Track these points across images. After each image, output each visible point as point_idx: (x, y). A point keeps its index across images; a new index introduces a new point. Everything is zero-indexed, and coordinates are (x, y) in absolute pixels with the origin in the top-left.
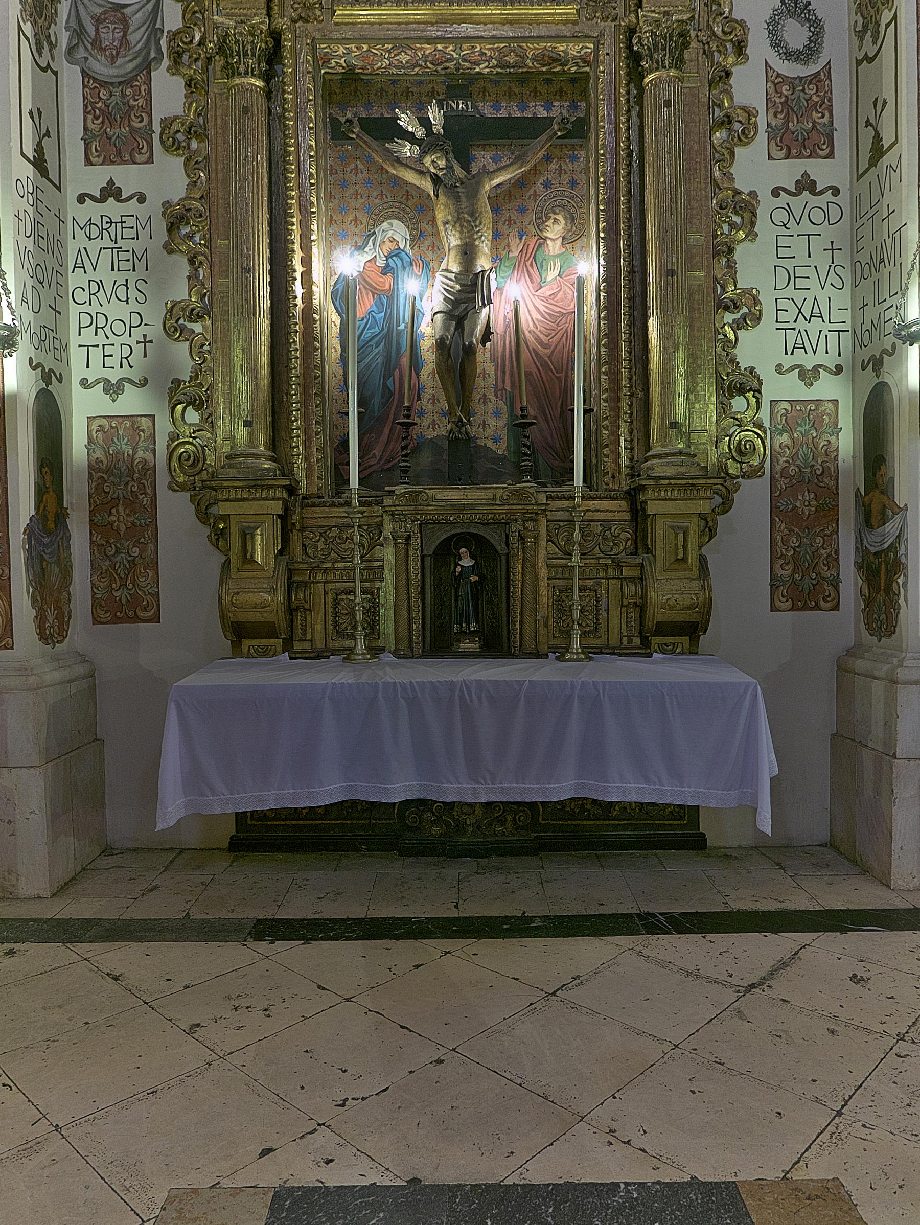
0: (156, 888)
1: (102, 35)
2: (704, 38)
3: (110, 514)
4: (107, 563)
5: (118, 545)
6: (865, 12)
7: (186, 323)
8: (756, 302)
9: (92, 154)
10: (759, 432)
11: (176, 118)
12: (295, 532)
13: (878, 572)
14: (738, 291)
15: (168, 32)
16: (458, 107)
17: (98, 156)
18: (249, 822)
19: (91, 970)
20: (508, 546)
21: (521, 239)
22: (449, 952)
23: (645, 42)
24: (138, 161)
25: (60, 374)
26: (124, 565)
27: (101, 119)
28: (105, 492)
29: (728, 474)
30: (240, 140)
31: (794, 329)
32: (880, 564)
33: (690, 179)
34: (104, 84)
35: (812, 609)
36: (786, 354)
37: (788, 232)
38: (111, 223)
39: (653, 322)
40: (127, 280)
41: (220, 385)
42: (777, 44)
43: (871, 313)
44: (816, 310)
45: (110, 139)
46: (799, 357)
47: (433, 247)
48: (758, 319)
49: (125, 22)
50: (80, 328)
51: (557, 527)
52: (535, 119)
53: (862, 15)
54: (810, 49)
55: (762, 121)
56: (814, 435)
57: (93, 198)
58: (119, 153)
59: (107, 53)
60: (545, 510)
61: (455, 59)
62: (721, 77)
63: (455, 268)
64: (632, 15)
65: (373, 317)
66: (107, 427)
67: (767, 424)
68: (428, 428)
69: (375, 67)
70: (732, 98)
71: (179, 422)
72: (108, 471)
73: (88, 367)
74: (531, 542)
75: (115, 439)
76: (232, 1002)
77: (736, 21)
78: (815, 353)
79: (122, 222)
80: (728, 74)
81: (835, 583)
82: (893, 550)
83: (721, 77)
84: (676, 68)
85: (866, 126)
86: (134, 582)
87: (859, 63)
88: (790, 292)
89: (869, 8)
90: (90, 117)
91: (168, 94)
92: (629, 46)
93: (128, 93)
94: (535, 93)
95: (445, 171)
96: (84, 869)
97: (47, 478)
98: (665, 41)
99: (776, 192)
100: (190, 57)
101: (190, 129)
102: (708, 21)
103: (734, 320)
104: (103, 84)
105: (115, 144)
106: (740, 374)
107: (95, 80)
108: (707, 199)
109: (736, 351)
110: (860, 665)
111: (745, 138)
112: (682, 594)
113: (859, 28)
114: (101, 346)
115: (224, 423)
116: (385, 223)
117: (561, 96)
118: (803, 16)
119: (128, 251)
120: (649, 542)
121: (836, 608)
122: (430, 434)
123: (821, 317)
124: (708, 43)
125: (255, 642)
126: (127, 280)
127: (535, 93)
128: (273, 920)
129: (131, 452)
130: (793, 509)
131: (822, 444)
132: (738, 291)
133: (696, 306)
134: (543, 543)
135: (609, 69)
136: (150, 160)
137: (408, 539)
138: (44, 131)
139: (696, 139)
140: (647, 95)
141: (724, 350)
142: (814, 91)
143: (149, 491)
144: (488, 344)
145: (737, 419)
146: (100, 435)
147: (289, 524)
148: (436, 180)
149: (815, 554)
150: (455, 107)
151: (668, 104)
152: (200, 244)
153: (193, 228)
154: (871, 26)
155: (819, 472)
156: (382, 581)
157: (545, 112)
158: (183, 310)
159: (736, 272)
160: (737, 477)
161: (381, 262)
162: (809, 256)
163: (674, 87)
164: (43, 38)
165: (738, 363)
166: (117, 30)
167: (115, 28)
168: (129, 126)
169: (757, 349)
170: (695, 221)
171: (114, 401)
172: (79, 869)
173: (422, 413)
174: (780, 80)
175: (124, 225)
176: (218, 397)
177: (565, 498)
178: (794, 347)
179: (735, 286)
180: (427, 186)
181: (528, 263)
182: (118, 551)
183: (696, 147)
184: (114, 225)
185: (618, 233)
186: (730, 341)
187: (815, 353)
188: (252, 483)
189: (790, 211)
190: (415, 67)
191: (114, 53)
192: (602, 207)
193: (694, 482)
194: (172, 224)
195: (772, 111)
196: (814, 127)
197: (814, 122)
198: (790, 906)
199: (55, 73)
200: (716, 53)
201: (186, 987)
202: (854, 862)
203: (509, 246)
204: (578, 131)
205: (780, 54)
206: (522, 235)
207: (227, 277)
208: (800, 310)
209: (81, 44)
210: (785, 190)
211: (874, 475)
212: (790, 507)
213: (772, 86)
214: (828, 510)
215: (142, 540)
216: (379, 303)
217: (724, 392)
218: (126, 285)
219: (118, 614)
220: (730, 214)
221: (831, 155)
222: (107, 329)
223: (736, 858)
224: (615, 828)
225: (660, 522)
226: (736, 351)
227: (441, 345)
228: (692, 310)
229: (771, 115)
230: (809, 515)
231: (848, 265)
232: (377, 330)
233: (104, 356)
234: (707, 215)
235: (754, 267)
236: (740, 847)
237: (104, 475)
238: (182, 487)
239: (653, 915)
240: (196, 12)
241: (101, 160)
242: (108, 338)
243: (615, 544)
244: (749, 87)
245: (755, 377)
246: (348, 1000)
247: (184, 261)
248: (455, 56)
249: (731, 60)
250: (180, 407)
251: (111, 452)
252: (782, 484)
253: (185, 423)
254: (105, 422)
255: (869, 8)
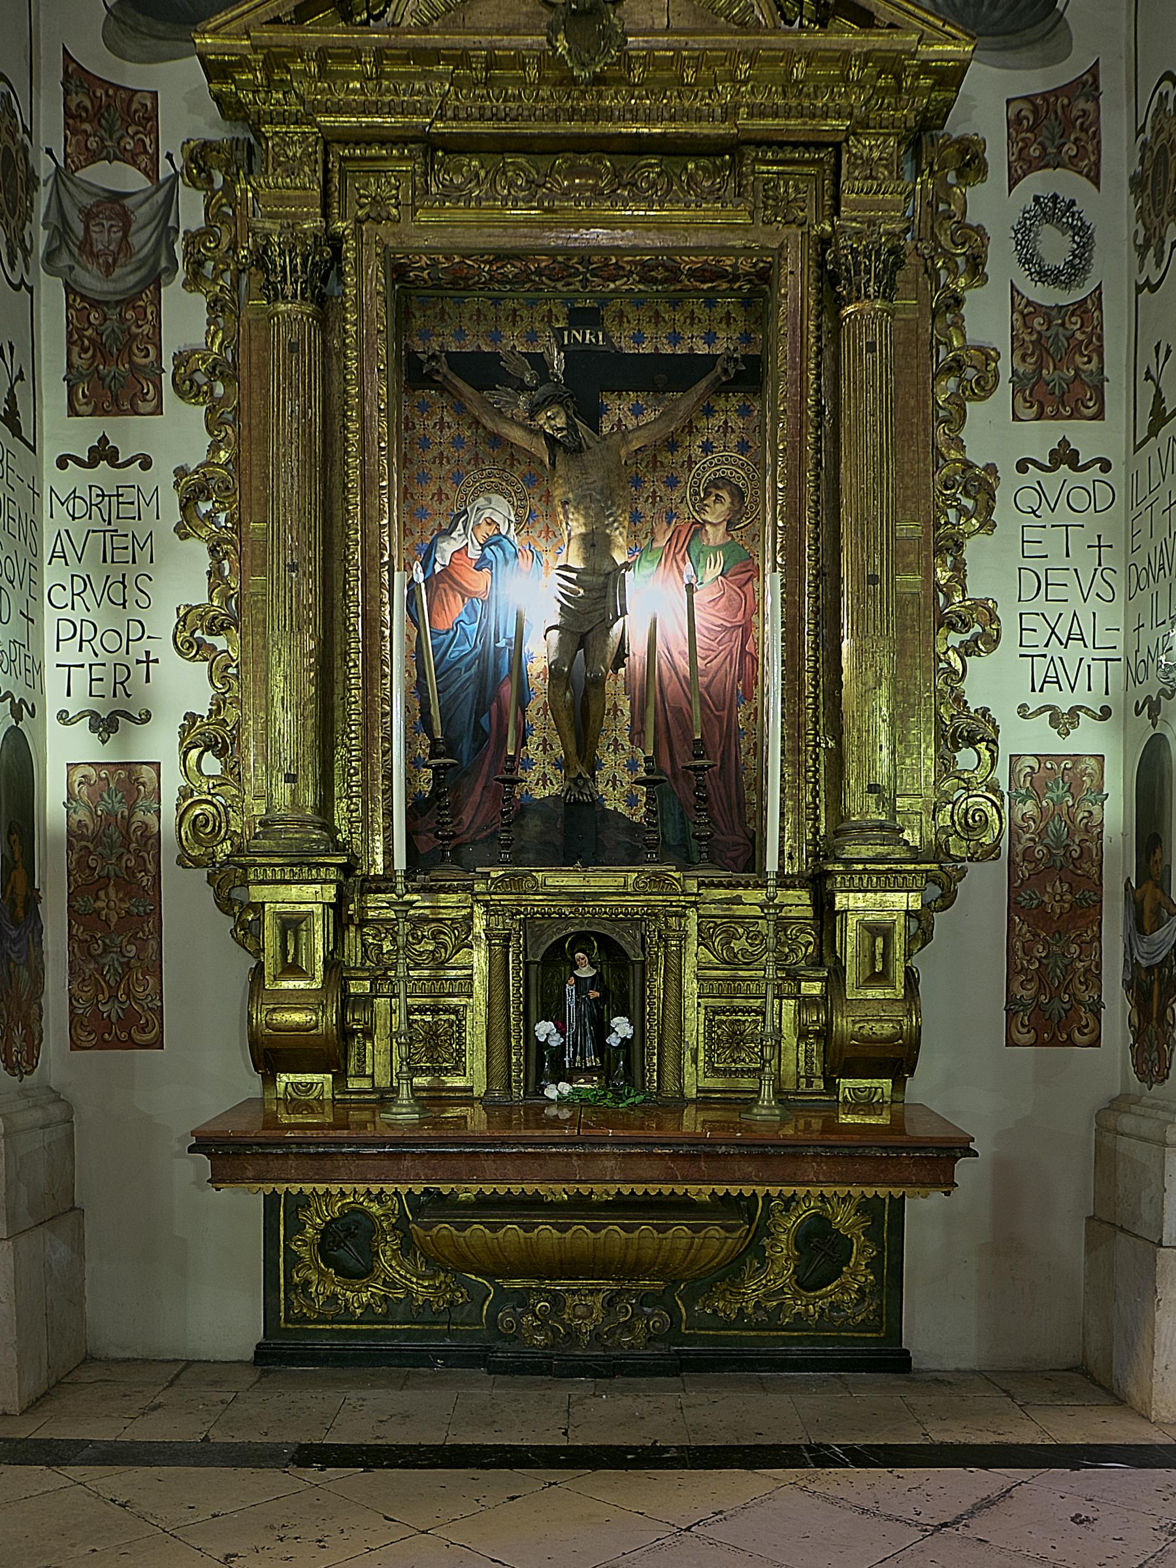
0: (160, 1406)
1: (94, 236)
2: (926, 251)
3: (97, 898)
4: (92, 966)
5: (107, 941)
6: (1148, 222)
7: (205, 637)
8: (993, 618)
9: (78, 400)
10: (994, 798)
11: (194, 352)
12: (352, 928)
13: (1150, 993)
14: (968, 603)
15: (185, 233)
16: (584, 339)
17: (86, 404)
18: (283, 1325)
19: (89, 1495)
20: (643, 949)
21: (669, 523)
22: (555, 1484)
23: (843, 260)
24: (142, 411)
25: (33, 706)
26: (116, 970)
27: (90, 352)
28: (89, 867)
29: (950, 856)
30: (284, 389)
31: (1044, 656)
32: (1152, 983)
33: (903, 447)
34: (95, 304)
35: (1063, 1044)
36: (1033, 690)
37: (1038, 522)
38: (103, 496)
39: (846, 645)
40: (124, 576)
41: (251, 722)
42: (1028, 259)
43: (1149, 637)
44: (1075, 630)
45: (103, 380)
46: (1051, 695)
47: (547, 533)
48: (994, 642)
49: (125, 218)
50: (58, 640)
51: (712, 925)
52: (692, 356)
53: (1144, 224)
54: (1073, 267)
55: (1005, 367)
56: (1070, 803)
57: (78, 461)
58: (115, 400)
59: (101, 261)
60: (694, 903)
61: (582, 273)
62: (948, 307)
63: (577, 563)
64: (827, 222)
65: (462, 628)
66: (94, 778)
67: (1004, 788)
68: (537, 784)
69: (470, 282)
70: (964, 336)
71: (193, 774)
72: (96, 839)
73: (69, 694)
74: (675, 946)
75: (105, 795)
76: (276, 1533)
77: (970, 227)
78: (1072, 689)
79: (118, 495)
80: (959, 302)
81: (1096, 1009)
82: (1168, 964)
83: (948, 307)
84: (884, 297)
85: (1146, 379)
86: (128, 994)
87: (1139, 289)
88: (1039, 605)
89: (1153, 216)
90: (76, 349)
91: (184, 320)
92: (821, 264)
93: (128, 317)
94: (693, 319)
95: (565, 433)
96: (59, 1382)
97: (16, 848)
98: (870, 260)
99: (1022, 466)
100: (214, 268)
101: (214, 368)
102: (932, 227)
103: (962, 642)
104: (95, 304)
105: (110, 388)
106: (968, 717)
107: (84, 298)
108: (927, 476)
109: (963, 686)
110: (1127, 1122)
111: (984, 387)
112: (880, 1020)
113: (1140, 241)
114: (87, 667)
115: (256, 776)
116: (481, 499)
117: (728, 324)
118: (1064, 220)
119: (126, 536)
120: (838, 950)
121: (1096, 1043)
122: (540, 793)
123: (1083, 639)
124: (932, 258)
125: (292, 1078)
126: (124, 576)
127: (693, 319)
128: (322, 1445)
129: (126, 813)
130: (1038, 906)
131: (1081, 816)
132: (968, 603)
133: (909, 623)
134: (692, 945)
135: (795, 287)
136: (158, 410)
137: (507, 939)
138: (16, 372)
139: (913, 391)
140: (844, 333)
141: (946, 684)
142: (1078, 326)
143: (151, 867)
144: (622, 670)
145: (963, 780)
146: (84, 788)
147: (344, 917)
148: (551, 441)
149: (1068, 968)
150: (580, 339)
151: (871, 347)
152: (226, 527)
153: (217, 505)
154: (1154, 242)
155: (1075, 855)
156: (470, 996)
157: (706, 346)
158: (202, 618)
159: (965, 576)
160: (962, 860)
161: (474, 553)
162: (1068, 555)
163: (880, 325)
164: (16, 243)
165: (966, 702)
166: (115, 229)
167: (112, 226)
168: (131, 362)
169: (993, 683)
170: (909, 504)
171: (104, 742)
172: (53, 1381)
173: (528, 764)
174: (1032, 309)
175: (121, 499)
176: (247, 739)
177: (723, 886)
178: (1045, 682)
179: (964, 596)
180: (540, 449)
181: (679, 557)
182: (106, 950)
183: (912, 402)
184: (107, 499)
185: (801, 520)
186: (955, 672)
187: (1072, 689)
188: (296, 860)
189: (1041, 494)
190: (526, 283)
191: (110, 260)
192: (780, 486)
193: (898, 867)
194: (188, 499)
195: (1019, 353)
196: (1077, 375)
197: (1077, 369)
198: (1013, 1439)
199: (30, 290)
200: (942, 272)
201: (214, 1516)
202: (1109, 1392)
203: (652, 532)
204: (749, 376)
205: (1031, 274)
206: (672, 518)
207: (263, 573)
208: (1053, 629)
209: (64, 248)
210: (1034, 462)
211: (1148, 861)
212: (1035, 902)
213: (1020, 319)
214: (1086, 909)
215: (141, 934)
216: (470, 609)
217: (946, 741)
218: (123, 583)
219: (106, 1035)
220: (958, 496)
221: (1099, 415)
222: (96, 643)
223: (950, 1383)
224: (786, 1341)
225: (852, 920)
226: (963, 686)
227: (555, 673)
228: (902, 628)
229: (1017, 359)
230: (1061, 913)
231: (1121, 570)
232: (467, 647)
233: (91, 680)
234: (927, 497)
235: (990, 569)
236: (958, 1371)
237: (89, 844)
238: (197, 863)
239: (828, 1447)
240: (224, 205)
241: (90, 409)
242: (96, 655)
243: (792, 950)
244: (987, 319)
245: (988, 722)
246: (423, 1532)
247: (204, 548)
248: (581, 269)
249: (962, 282)
250: (194, 753)
251: (99, 813)
252: (1025, 870)
253: (202, 774)
254: (91, 771)
255: (1153, 216)
